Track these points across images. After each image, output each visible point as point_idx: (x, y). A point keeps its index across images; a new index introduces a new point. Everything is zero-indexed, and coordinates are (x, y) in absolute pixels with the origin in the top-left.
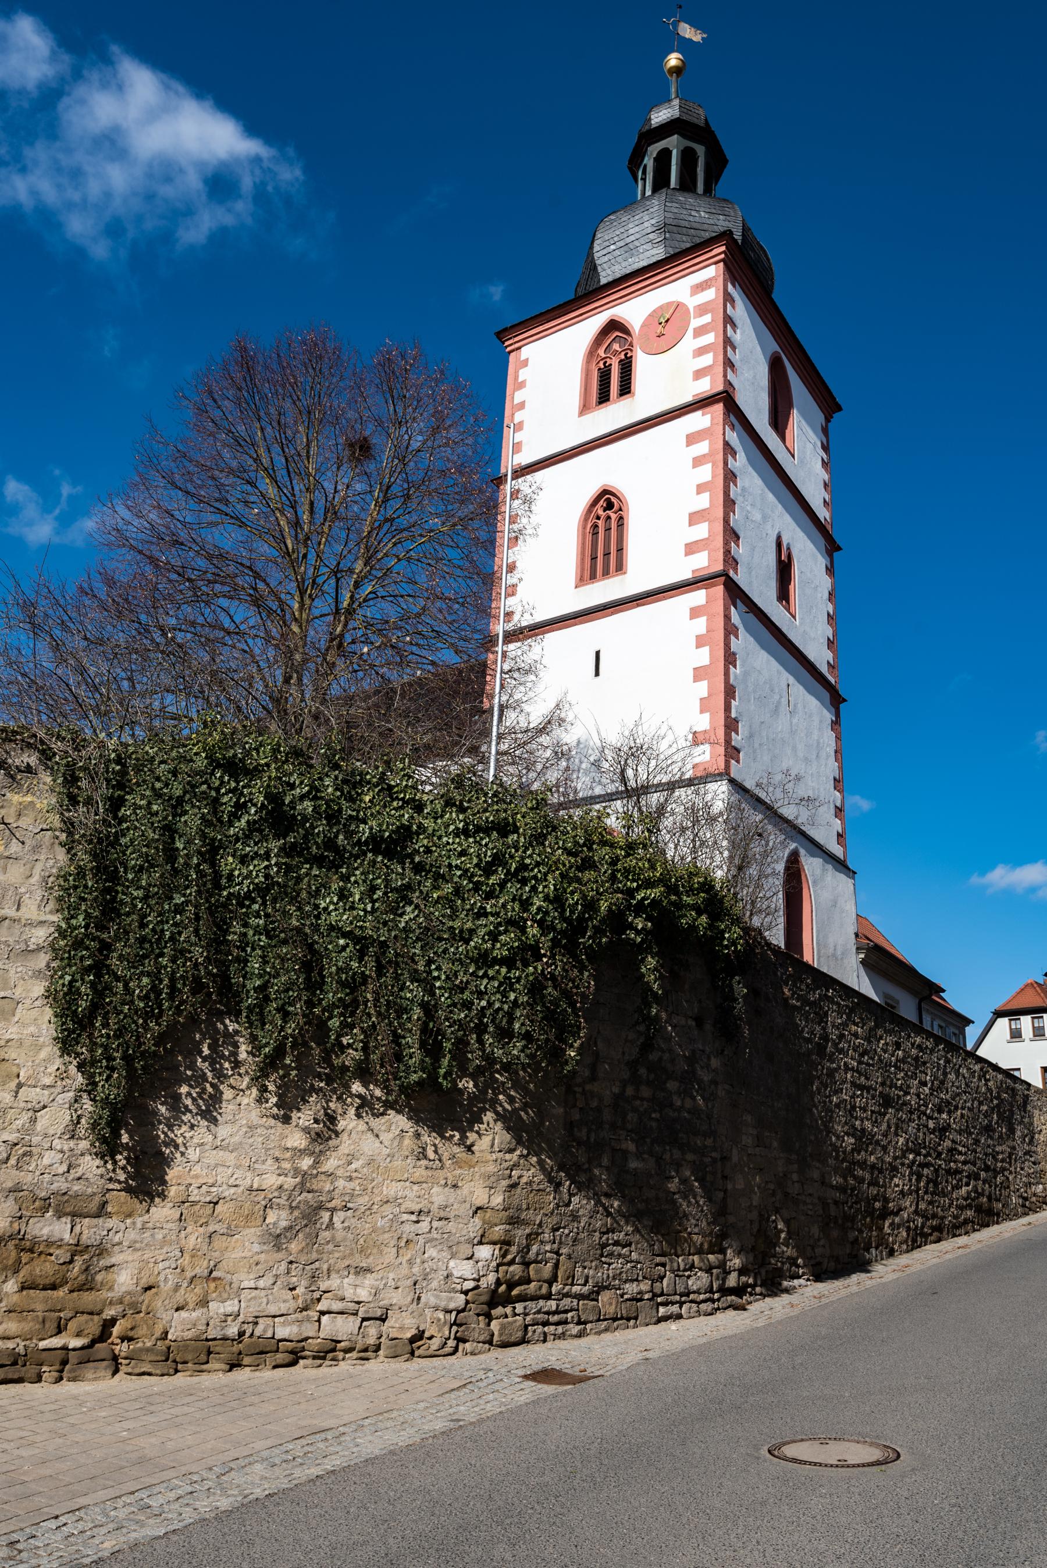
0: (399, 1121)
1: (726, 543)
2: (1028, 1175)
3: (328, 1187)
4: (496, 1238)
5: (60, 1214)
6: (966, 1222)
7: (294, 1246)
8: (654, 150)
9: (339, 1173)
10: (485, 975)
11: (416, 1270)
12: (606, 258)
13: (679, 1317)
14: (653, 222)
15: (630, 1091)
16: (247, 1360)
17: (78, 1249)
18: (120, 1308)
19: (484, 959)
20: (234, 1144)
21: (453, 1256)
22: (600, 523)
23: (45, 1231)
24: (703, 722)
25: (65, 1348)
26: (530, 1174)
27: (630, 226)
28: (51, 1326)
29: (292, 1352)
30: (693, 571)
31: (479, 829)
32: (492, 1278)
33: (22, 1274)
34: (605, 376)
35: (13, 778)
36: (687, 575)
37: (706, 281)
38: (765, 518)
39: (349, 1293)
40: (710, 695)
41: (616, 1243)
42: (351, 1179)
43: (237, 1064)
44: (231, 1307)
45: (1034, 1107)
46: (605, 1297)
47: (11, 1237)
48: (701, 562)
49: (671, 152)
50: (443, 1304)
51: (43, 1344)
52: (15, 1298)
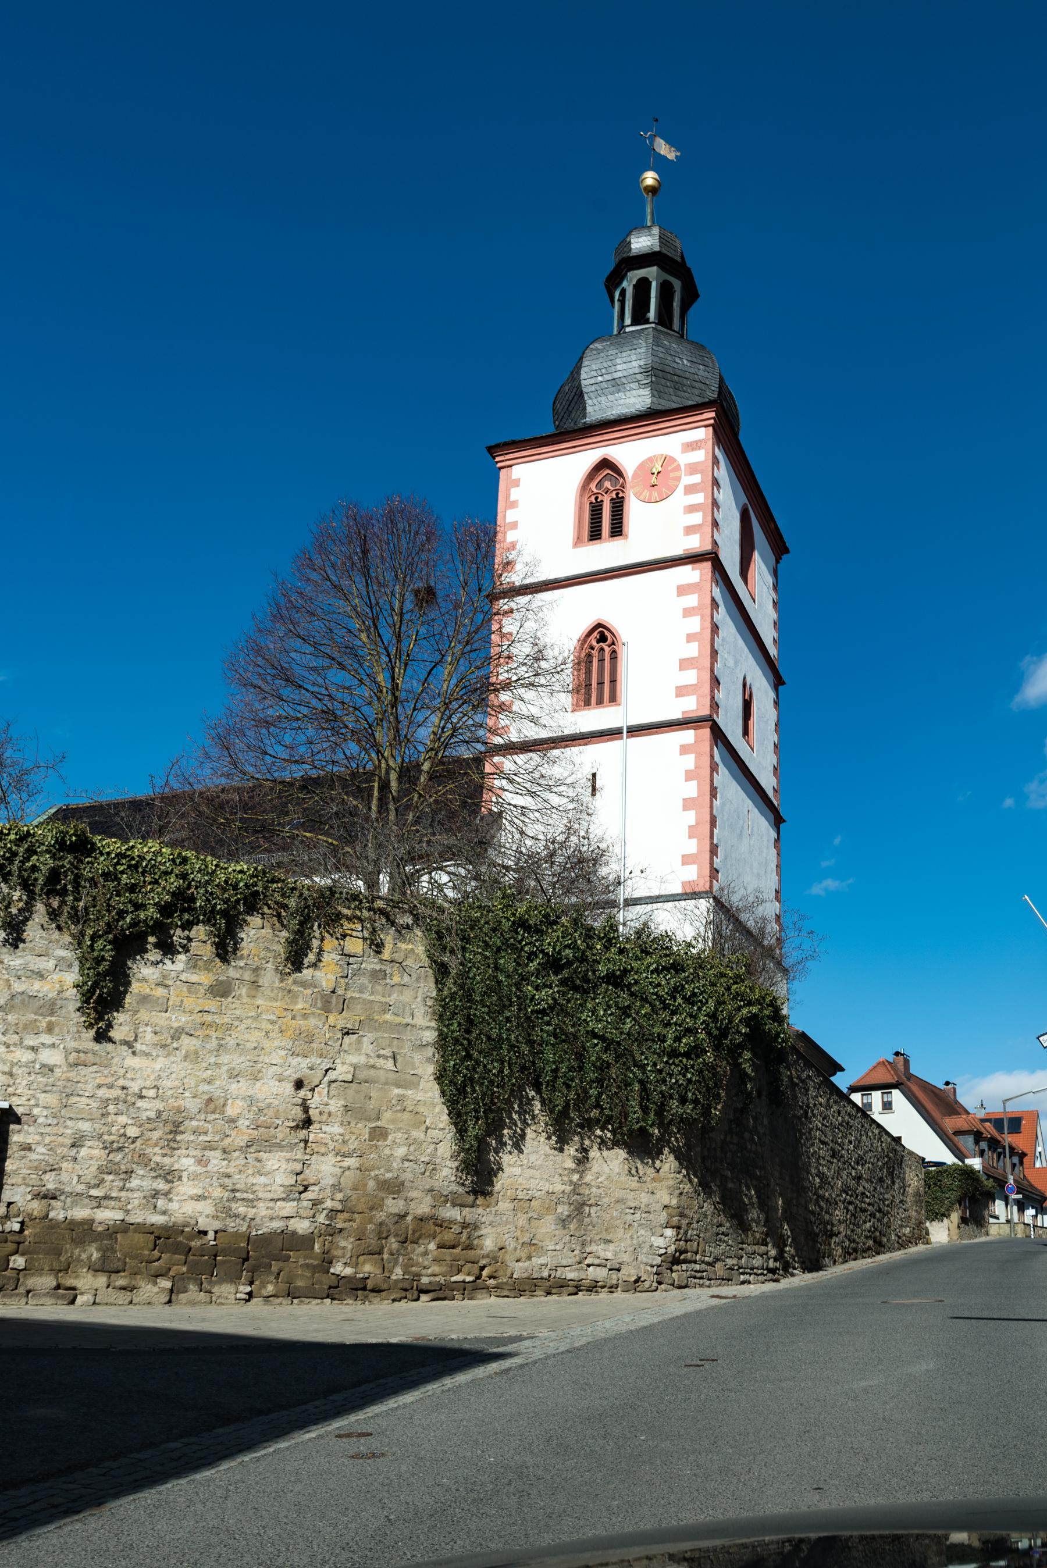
0: (621, 1154)
1: (712, 691)
2: (901, 1219)
3: (587, 1192)
4: (674, 1224)
5: (454, 1205)
6: (869, 1248)
7: (572, 1226)
8: (635, 275)
9: (593, 1183)
10: (673, 1063)
11: (635, 1242)
12: (593, 388)
13: (749, 1283)
14: (642, 363)
15: (728, 1139)
16: (554, 1291)
17: (465, 1225)
18: (488, 1260)
19: (674, 1053)
20: (533, 1165)
21: (653, 1234)
22: (594, 653)
23: (448, 1215)
24: (692, 846)
25: (464, 1282)
26: (687, 1187)
27: (618, 361)
28: (455, 1269)
29: (576, 1287)
30: (683, 713)
31: (664, 968)
32: (673, 1248)
33: (437, 1239)
34: (596, 510)
35: (400, 932)
36: (676, 715)
37: (697, 442)
38: (736, 662)
39: (602, 1254)
40: (697, 823)
41: (723, 1234)
42: (599, 1187)
43: (534, 1117)
44: (542, 1260)
45: (907, 1166)
46: (718, 1265)
47: (432, 1218)
48: (691, 705)
49: (650, 283)
50: (650, 1262)
51: (453, 1279)
52: (435, 1253)
